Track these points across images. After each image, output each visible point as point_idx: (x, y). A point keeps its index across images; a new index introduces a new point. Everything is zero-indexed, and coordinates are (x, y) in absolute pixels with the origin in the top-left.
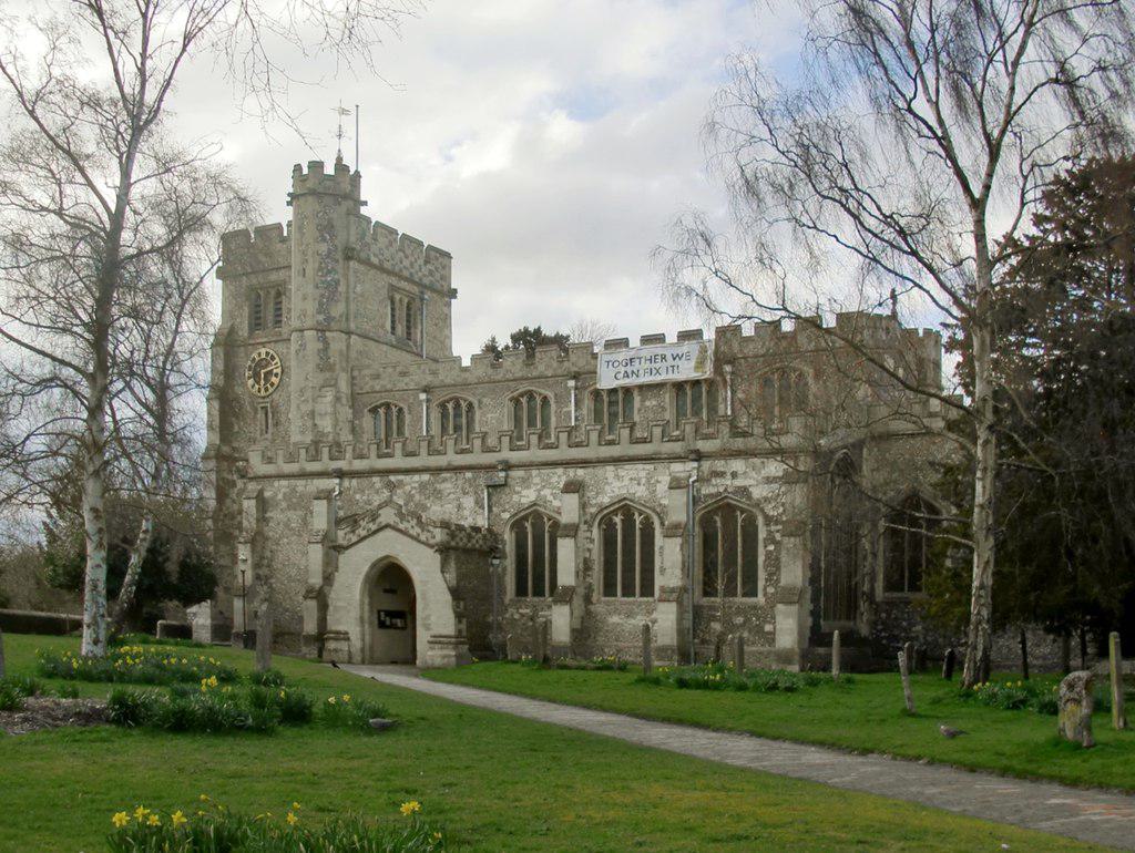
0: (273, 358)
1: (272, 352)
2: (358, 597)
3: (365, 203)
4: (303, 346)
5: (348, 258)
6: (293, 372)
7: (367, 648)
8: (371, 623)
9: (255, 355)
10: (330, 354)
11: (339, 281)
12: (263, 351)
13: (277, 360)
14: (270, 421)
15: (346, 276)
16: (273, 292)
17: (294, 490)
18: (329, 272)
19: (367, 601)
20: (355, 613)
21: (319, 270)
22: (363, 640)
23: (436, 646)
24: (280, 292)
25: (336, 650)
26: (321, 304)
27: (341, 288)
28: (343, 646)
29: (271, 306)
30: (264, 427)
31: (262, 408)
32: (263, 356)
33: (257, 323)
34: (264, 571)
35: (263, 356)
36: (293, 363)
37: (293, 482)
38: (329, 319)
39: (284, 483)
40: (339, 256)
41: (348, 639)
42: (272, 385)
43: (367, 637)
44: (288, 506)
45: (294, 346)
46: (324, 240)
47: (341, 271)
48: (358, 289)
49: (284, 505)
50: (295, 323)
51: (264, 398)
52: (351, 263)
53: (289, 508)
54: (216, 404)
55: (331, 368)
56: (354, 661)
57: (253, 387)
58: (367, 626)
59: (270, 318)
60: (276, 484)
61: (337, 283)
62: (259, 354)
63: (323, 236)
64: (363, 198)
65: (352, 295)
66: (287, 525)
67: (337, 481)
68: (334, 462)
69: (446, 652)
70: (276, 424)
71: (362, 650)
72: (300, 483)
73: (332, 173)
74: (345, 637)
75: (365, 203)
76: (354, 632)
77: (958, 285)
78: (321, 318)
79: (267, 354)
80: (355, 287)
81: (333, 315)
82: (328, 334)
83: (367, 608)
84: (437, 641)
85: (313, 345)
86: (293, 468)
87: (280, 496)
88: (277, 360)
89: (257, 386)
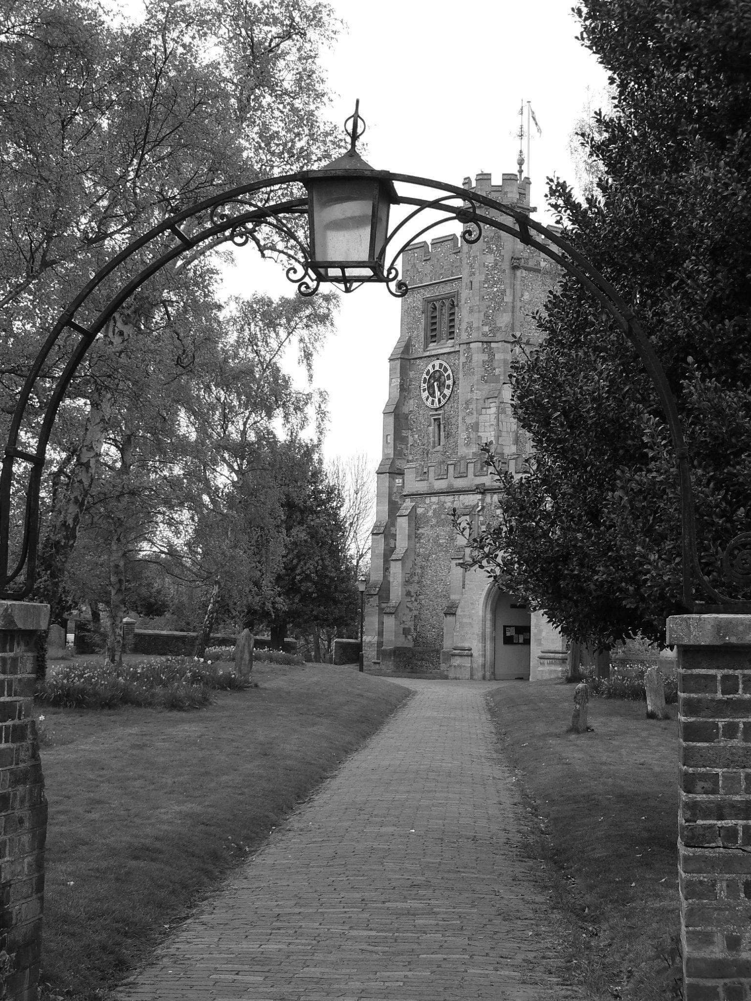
0: (446, 370)
1: (445, 364)
2: (481, 613)
3: (534, 209)
4: (469, 359)
5: (515, 268)
6: (461, 382)
7: (488, 665)
8: (494, 639)
9: (430, 367)
10: (495, 365)
11: (505, 291)
12: (437, 363)
13: (449, 372)
14: (442, 433)
15: (513, 287)
16: (447, 303)
17: (442, 505)
18: (496, 283)
19: (489, 616)
20: (477, 629)
21: (485, 282)
22: (484, 656)
23: (546, 661)
24: (452, 302)
25: (460, 666)
26: (487, 316)
27: (508, 298)
28: (466, 662)
29: (446, 318)
30: (437, 439)
31: (435, 420)
32: (437, 368)
33: (433, 336)
34: (413, 588)
35: (437, 368)
36: (461, 376)
37: (442, 498)
38: (495, 330)
39: (434, 499)
40: (506, 266)
41: (471, 655)
42: (444, 396)
43: (488, 653)
44: (437, 522)
45: (463, 359)
46: (491, 251)
47: (507, 281)
48: (526, 296)
49: (434, 521)
50: (464, 337)
51: (436, 410)
52: (519, 273)
53: (438, 525)
54: (391, 419)
55: (496, 379)
56: (475, 677)
57: (427, 400)
58: (488, 643)
59: (445, 329)
60: (427, 501)
61: (503, 292)
62: (434, 366)
63: (490, 248)
64: (532, 205)
65: (518, 304)
66: (436, 542)
67: (479, 496)
68: (478, 478)
69: (553, 668)
70: (448, 436)
71: (484, 666)
72: (449, 499)
73: (500, 183)
74: (467, 653)
75: (534, 209)
76: (476, 646)
77: (311, 638)
78: (486, 329)
79: (441, 365)
80: (522, 295)
81: (499, 325)
82: (493, 345)
83: (489, 624)
84: (546, 657)
85: (479, 358)
86: (441, 485)
87: (430, 513)
88: (449, 372)
89: (430, 399)
